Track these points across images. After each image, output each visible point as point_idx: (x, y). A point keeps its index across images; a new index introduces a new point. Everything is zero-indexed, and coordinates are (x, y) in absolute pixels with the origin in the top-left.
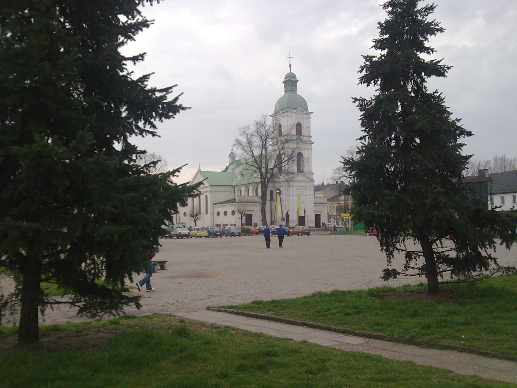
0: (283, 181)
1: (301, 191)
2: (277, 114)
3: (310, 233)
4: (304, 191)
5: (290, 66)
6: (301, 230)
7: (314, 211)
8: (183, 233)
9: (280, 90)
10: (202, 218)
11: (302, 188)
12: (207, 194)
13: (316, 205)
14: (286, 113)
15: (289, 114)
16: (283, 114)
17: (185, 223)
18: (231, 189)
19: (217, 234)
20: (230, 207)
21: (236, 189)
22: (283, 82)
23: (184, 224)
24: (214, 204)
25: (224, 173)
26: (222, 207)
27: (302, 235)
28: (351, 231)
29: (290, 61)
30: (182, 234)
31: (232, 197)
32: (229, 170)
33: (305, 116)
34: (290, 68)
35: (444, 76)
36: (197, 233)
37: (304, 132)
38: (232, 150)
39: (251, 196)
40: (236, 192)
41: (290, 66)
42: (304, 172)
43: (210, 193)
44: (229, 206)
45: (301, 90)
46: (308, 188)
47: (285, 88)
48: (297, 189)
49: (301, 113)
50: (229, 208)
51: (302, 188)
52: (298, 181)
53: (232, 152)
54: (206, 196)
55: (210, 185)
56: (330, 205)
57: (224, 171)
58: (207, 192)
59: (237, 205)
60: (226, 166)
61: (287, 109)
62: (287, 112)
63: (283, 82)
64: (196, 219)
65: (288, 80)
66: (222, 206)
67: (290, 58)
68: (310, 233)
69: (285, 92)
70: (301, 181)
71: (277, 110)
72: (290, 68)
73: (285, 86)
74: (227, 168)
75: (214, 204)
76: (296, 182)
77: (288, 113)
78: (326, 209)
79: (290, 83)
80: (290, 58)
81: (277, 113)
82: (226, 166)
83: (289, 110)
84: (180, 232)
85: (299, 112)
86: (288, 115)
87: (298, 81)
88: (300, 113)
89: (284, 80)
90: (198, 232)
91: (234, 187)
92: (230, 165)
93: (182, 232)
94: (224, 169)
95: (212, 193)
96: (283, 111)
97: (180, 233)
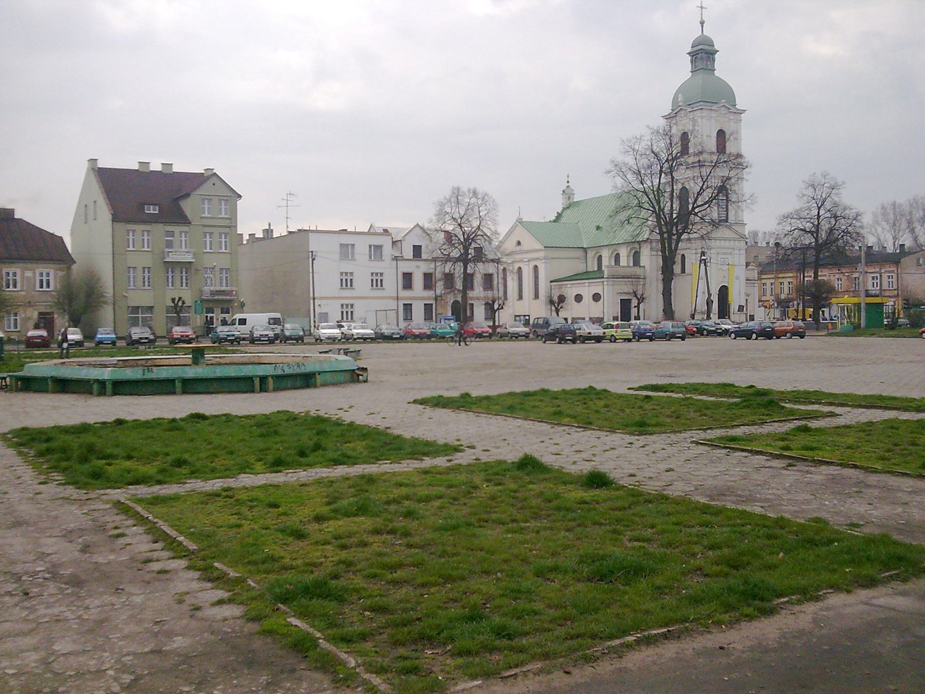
0: (695, 239)
1: (725, 256)
2: (679, 113)
3: (807, 334)
4: (729, 256)
5: (702, 23)
6: (791, 328)
7: (745, 293)
8: (594, 333)
9: (683, 70)
10: (570, 307)
11: (726, 251)
12: (521, 265)
13: (748, 285)
14: (700, 111)
15: (705, 113)
16: (692, 113)
17: (529, 316)
18: (580, 253)
19: (647, 334)
20: (589, 286)
21: (590, 254)
22: (688, 53)
23: (527, 318)
24: (551, 282)
25: (553, 223)
26: (589, 286)
27: (793, 337)
28: (864, 329)
29: (702, 14)
30: (593, 335)
31: (580, 268)
32: (562, 219)
33: (731, 118)
34: (702, 27)
35: (88, 161)
36: (615, 334)
37: (730, 148)
38: (568, 182)
39: (624, 267)
40: (589, 259)
41: (702, 23)
42: (729, 221)
43: (543, 261)
44: (587, 284)
45: (722, 68)
46: (737, 252)
47: (692, 64)
48: (718, 253)
49: (726, 111)
50: (587, 288)
51: (726, 251)
52: (720, 239)
53: (568, 187)
54: (536, 267)
55: (545, 247)
56: (772, 281)
57: (554, 221)
58: (538, 259)
59: (605, 283)
60: (558, 213)
61: (701, 103)
62: (701, 109)
63: (688, 53)
64: (559, 307)
65: (701, 49)
66: (587, 284)
67: (702, 7)
68: (805, 333)
69: (692, 72)
70: (725, 239)
71: (679, 106)
72: (702, 27)
73: (692, 62)
74: (559, 216)
75: (551, 282)
76: (715, 239)
77: (704, 111)
78: (757, 289)
79: (703, 54)
80: (702, 7)
81: (679, 111)
82: (558, 213)
83: (706, 106)
84: (589, 331)
85: (723, 109)
86: (704, 114)
87: (718, 51)
88: (723, 111)
89: (689, 50)
90: (616, 331)
91: (585, 250)
92: (564, 209)
93: (592, 332)
94: (554, 218)
95: (549, 261)
96: (693, 108)
97: (590, 333)
